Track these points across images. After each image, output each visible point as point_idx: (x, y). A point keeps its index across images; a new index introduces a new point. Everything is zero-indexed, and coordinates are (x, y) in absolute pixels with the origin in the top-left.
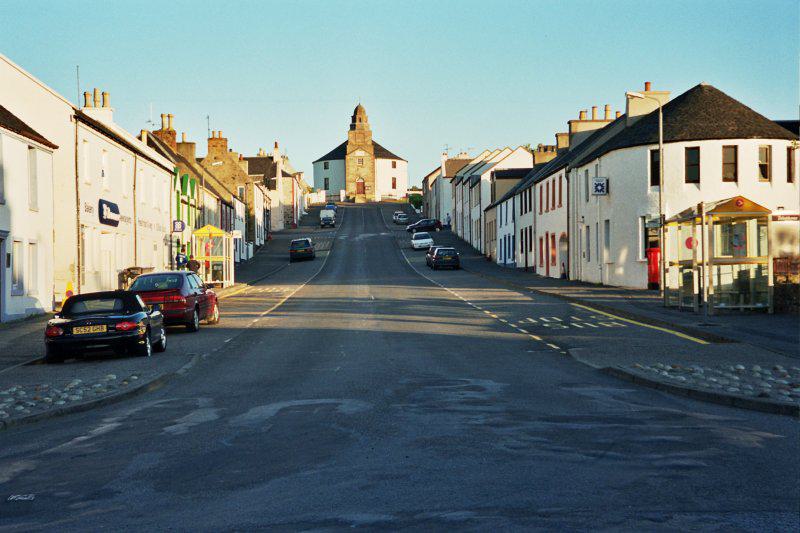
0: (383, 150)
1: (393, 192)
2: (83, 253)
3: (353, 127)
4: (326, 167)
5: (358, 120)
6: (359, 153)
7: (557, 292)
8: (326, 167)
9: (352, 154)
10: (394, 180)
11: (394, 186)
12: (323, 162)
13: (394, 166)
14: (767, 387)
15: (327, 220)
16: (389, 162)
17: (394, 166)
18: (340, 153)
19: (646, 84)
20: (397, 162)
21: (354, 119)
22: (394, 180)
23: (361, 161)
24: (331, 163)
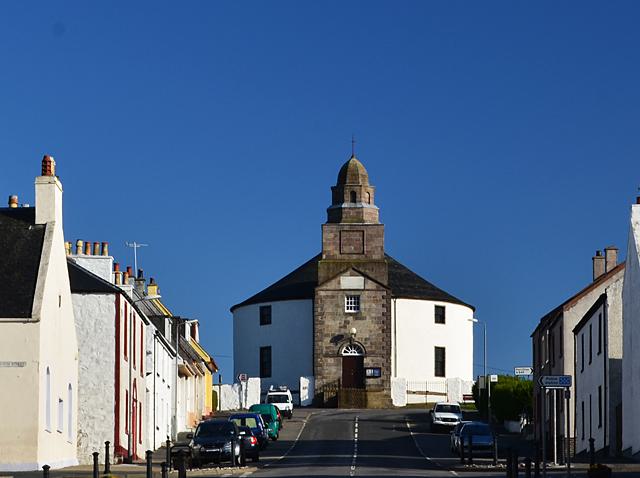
0: (411, 277)
1: (438, 384)
2: (606, 345)
3: (335, 216)
4: (266, 318)
5: (347, 196)
6: (351, 281)
7: (633, 465)
8: (266, 318)
9: (332, 285)
10: (440, 353)
11: (440, 370)
12: (256, 308)
13: (440, 316)
14: (332, 235)
15: (249, 458)
16: (428, 307)
17: (440, 316)
18: (302, 285)
20: (450, 308)
21: (338, 195)
22: (440, 353)
23: (356, 297)
24: (279, 308)
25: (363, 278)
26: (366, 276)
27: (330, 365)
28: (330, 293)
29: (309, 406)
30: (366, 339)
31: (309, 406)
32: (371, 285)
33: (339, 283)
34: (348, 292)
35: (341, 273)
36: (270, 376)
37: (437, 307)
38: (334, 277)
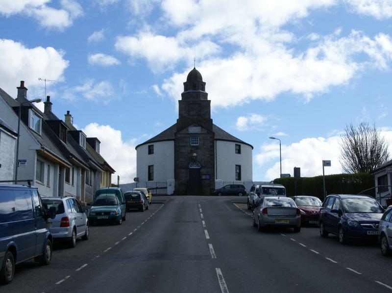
4: (151, 151)
8: (151, 151)
10: (150, 168)
13: (239, 151)
19: (149, 167)
22: (239, 167)
25: (200, 127)
26: (202, 127)
27: (374, 211)
28: (183, 136)
29: (172, 195)
30: (202, 160)
31: (172, 195)
32: (205, 131)
33: (188, 130)
34: (192, 135)
35: (189, 125)
36: (153, 180)
37: (236, 145)
38: (185, 128)
